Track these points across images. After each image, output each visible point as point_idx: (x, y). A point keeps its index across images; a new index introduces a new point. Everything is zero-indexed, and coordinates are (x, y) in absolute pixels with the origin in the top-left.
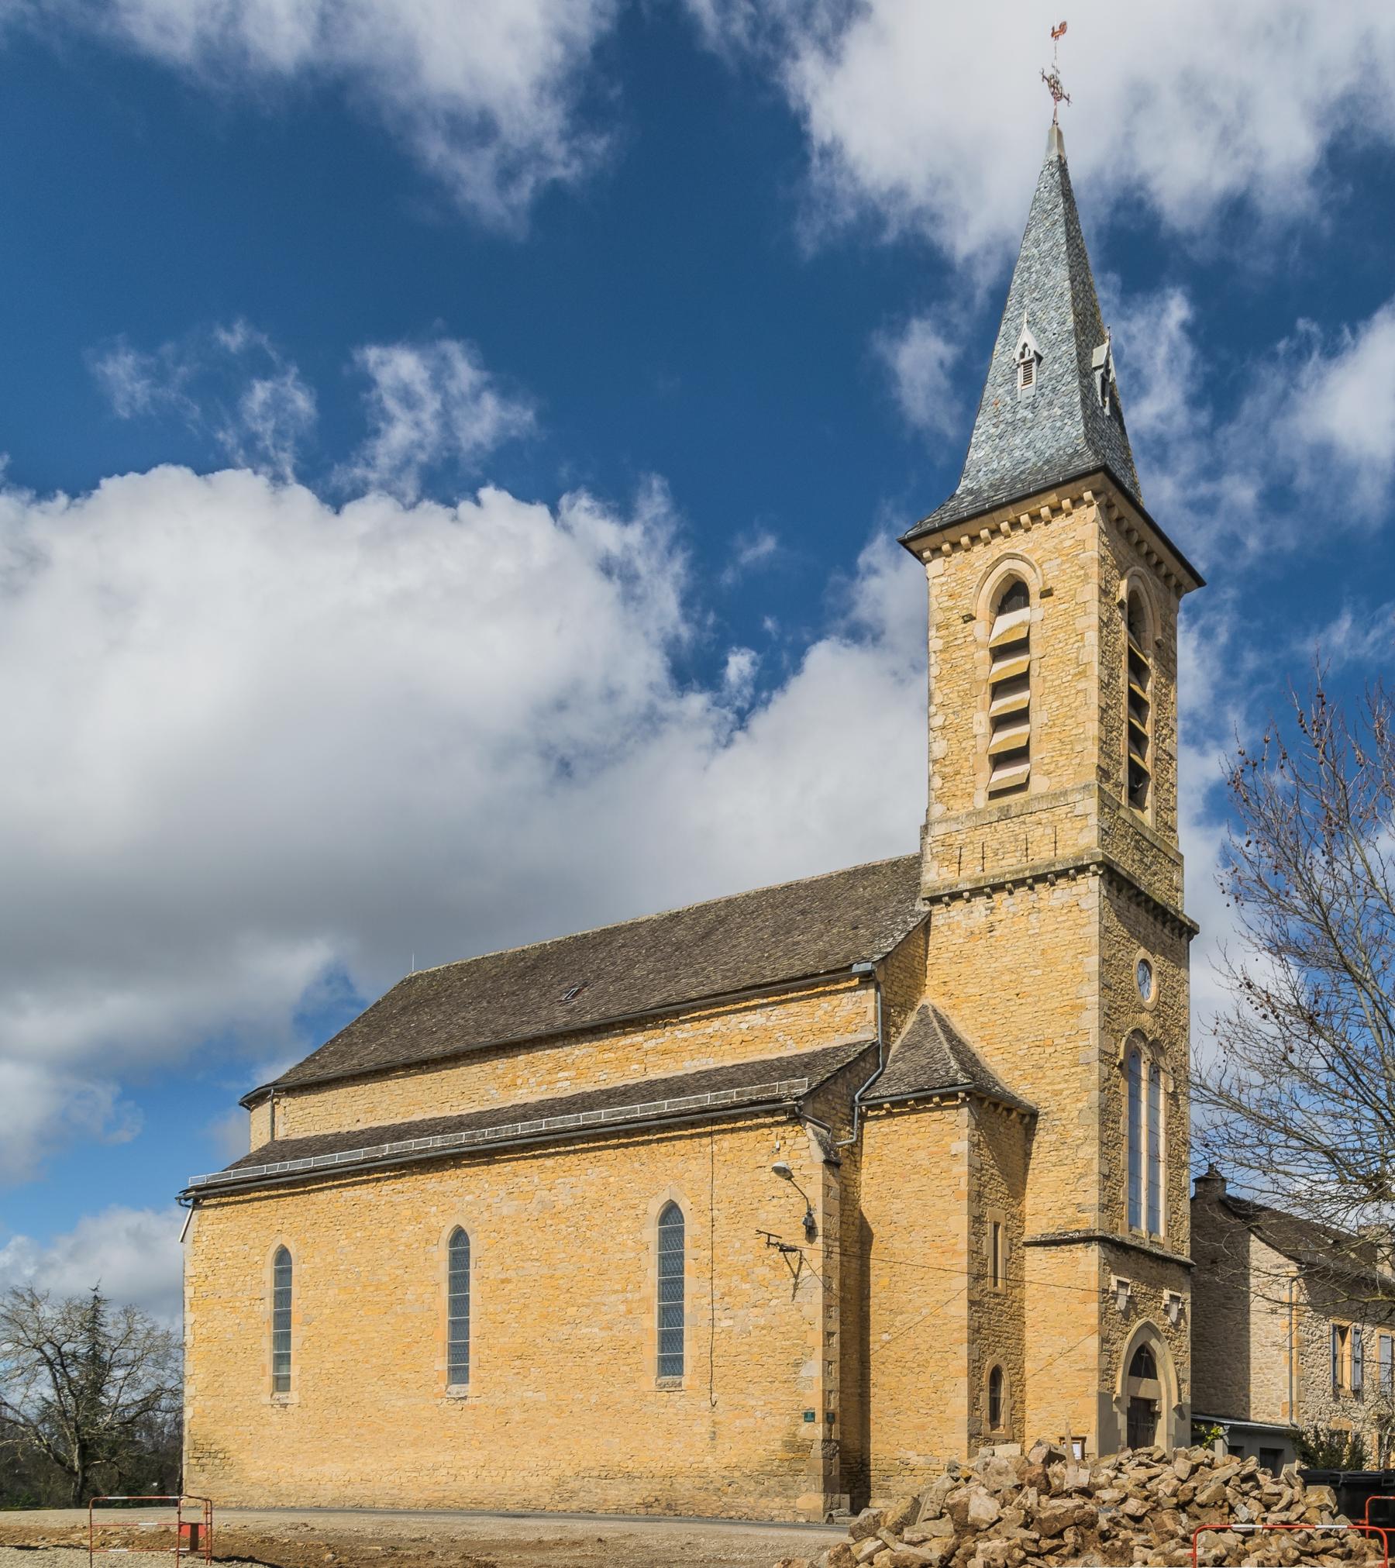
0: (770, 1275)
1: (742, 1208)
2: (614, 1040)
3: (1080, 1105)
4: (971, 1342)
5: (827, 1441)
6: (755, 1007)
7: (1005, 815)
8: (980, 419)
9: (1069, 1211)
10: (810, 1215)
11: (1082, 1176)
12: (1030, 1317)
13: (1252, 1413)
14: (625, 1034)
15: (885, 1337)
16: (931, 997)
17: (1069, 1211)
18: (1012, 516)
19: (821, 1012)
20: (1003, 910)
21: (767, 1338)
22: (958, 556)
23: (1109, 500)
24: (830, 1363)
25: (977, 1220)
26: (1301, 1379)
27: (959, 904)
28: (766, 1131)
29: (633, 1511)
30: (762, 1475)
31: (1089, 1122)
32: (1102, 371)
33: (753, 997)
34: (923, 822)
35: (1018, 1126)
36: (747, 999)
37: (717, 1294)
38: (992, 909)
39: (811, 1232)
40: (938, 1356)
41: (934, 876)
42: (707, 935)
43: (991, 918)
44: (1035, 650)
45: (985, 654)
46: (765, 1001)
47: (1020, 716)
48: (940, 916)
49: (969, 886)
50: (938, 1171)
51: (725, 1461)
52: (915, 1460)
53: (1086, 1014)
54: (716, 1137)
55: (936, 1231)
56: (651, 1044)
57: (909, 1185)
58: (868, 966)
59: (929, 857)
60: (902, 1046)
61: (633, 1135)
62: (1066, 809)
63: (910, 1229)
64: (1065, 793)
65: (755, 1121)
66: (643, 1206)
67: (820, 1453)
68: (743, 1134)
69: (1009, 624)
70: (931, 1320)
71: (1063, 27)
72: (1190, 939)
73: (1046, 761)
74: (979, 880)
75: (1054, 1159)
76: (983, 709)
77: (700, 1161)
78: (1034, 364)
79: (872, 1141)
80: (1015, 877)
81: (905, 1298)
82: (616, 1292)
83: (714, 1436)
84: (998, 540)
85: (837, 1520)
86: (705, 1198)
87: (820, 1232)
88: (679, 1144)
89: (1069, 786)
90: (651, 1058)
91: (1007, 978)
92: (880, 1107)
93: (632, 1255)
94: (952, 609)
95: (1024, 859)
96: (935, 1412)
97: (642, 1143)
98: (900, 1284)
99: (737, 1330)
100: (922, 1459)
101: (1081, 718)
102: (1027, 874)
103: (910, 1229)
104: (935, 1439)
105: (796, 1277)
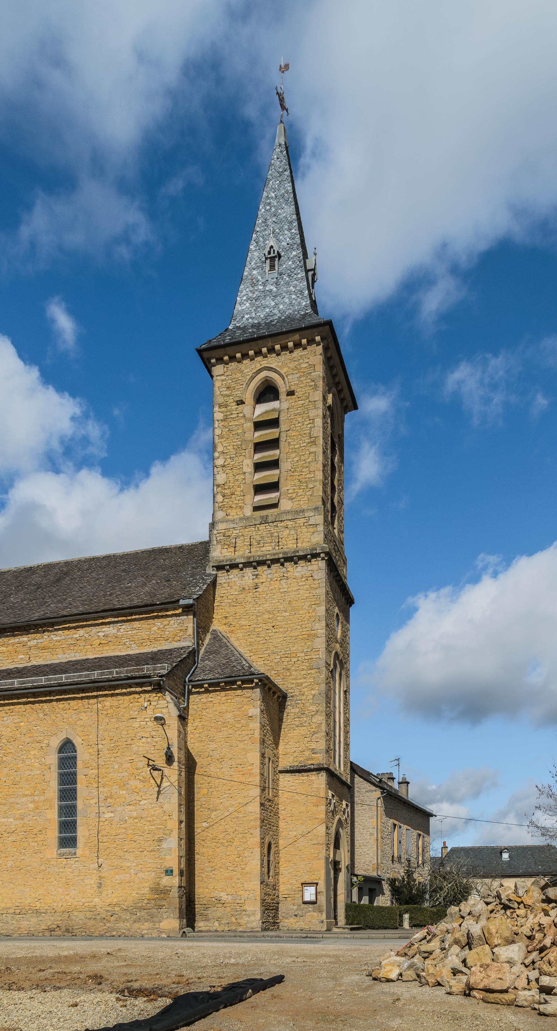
0: (140, 785)
1: (120, 743)
2: (6, 640)
3: (313, 692)
4: (261, 827)
5: (180, 887)
6: (109, 623)
7: (265, 521)
8: (242, 287)
9: (307, 753)
10: (169, 748)
11: (314, 733)
12: (282, 814)
13: (356, 869)
14: (14, 636)
15: (205, 824)
16: (217, 625)
17: (307, 753)
18: (270, 344)
19: (155, 628)
20: (264, 576)
21: (138, 825)
22: (233, 365)
23: (328, 344)
24: (181, 839)
25: (263, 755)
26: (382, 851)
27: (235, 571)
28: (137, 696)
29: (41, 934)
30: (137, 910)
31: (319, 702)
32: (312, 272)
33: (107, 617)
34: (210, 521)
35: (276, 703)
36: (103, 618)
37: (102, 797)
38: (257, 575)
39: (169, 759)
40: (240, 836)
41: (218, 553)
42: (58, 580)
43: (256, 581)
44: (283, 426)
45: (250, 425)
46: (116, 619)
47: (274, 464)
48: (222, 577)
49: (243, 561)
50: (240, 726)
51: (108, 901)
52: (224, 897)
53: (317, 639)
54: (100, 699)
55: (239, 761)
56: (33, 643)
57: (219, 734)
58: (191, 601)
59: (215, 542)
60: (206, 652)
61: (38, 696)
62: (303, 520)
63: (221, 760)
64: (303, 511)
65: (128, 690)
66: (47, 742)
67: (177, 895)
68: (120, 697)
69: (262, 410)
70: (235, 814)
71: (287, 66)
72: (351, 606)
73: (290, 491)
74: (249, 558)
75: (297, 723)
76: (250, 458)
77: (89, 714)
78: (277, 259)
79: (195, 707)
80: (273, 557)
81: (218, 801)
82: (27, 795)
83: (100, 886)
84: (259, 358)
85: (188, 935)
86: (93, 737)
87: (176, 759)
88: (72, 703)
89: (305, 507)
90: (33, 651)
91: (266, 616)
92: (201, 686)
93: (38, 772)
94: (229, 396)
95: (277, 548)
96: (238, 869)
97: (45, 702)
98: (215, 793)
99: (117, 819)
100: (230, 897)
101: (312, 469)
102: (281, 556)
103: (221, 760)
104: (239, 885)
105: (159, 786)
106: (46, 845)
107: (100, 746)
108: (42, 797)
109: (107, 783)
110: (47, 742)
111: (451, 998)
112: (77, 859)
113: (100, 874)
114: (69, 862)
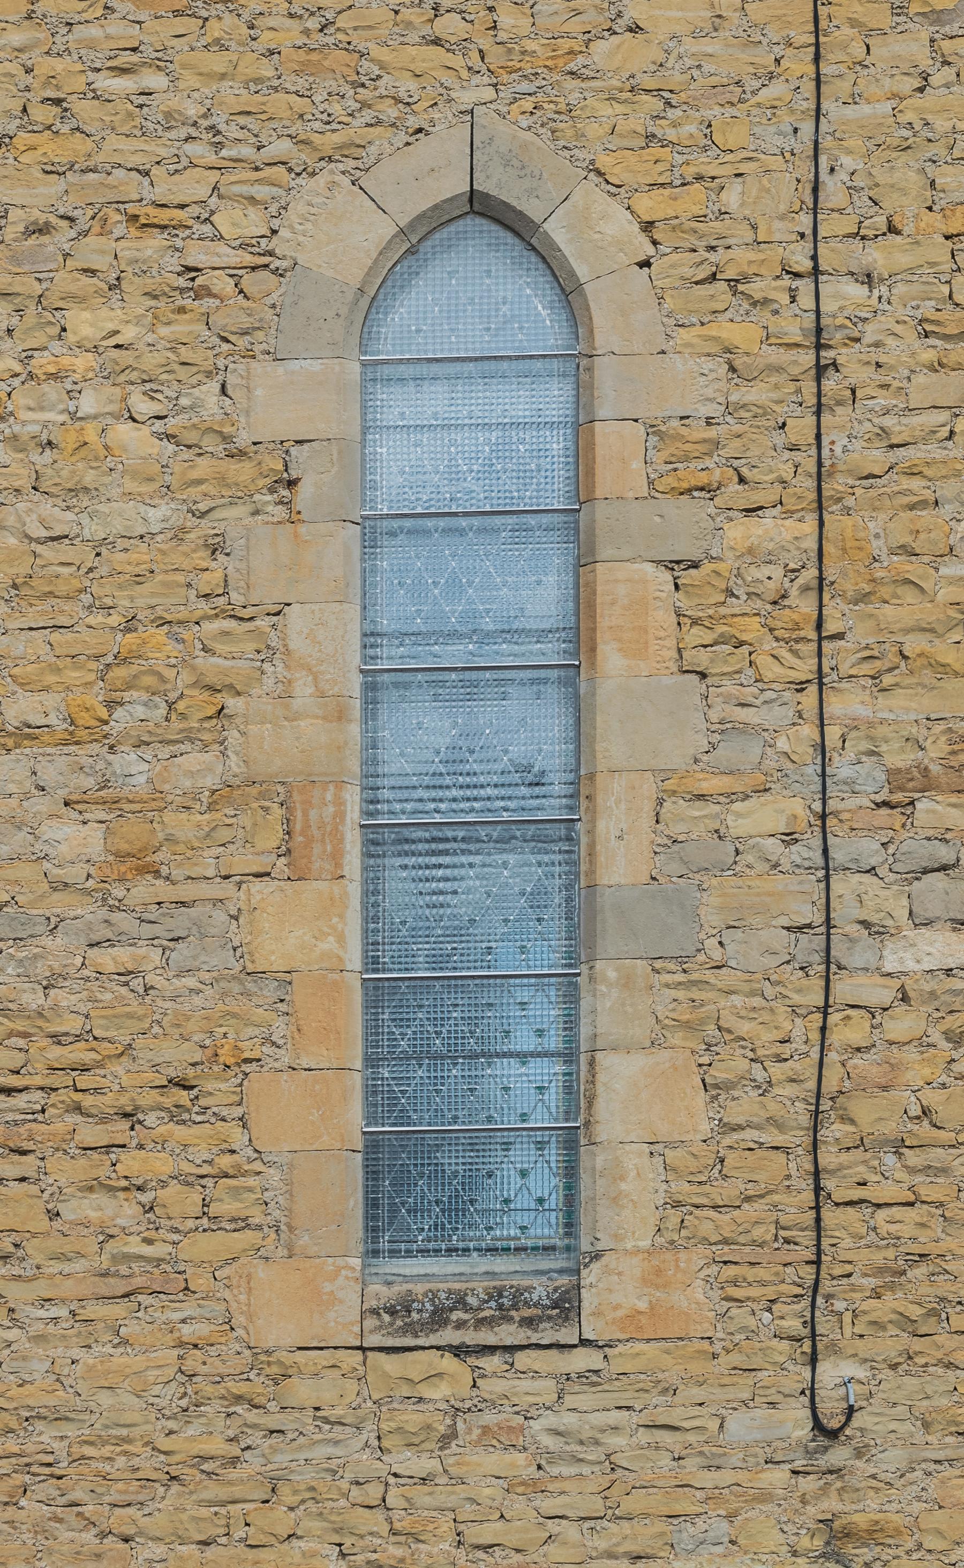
86: (764, 200)
93: (160, 514)
106: (242, 1223)
107: (840, 296)
108: (194, 759)
109: (914, 644)
110: (253, 223)
111: (211, 1552)
112: (582, 1360)
113: (832, 1504)
114: (490, 1387)
